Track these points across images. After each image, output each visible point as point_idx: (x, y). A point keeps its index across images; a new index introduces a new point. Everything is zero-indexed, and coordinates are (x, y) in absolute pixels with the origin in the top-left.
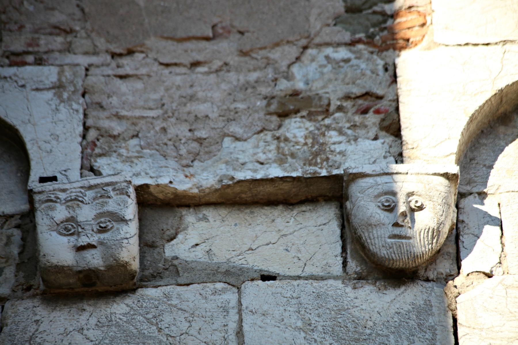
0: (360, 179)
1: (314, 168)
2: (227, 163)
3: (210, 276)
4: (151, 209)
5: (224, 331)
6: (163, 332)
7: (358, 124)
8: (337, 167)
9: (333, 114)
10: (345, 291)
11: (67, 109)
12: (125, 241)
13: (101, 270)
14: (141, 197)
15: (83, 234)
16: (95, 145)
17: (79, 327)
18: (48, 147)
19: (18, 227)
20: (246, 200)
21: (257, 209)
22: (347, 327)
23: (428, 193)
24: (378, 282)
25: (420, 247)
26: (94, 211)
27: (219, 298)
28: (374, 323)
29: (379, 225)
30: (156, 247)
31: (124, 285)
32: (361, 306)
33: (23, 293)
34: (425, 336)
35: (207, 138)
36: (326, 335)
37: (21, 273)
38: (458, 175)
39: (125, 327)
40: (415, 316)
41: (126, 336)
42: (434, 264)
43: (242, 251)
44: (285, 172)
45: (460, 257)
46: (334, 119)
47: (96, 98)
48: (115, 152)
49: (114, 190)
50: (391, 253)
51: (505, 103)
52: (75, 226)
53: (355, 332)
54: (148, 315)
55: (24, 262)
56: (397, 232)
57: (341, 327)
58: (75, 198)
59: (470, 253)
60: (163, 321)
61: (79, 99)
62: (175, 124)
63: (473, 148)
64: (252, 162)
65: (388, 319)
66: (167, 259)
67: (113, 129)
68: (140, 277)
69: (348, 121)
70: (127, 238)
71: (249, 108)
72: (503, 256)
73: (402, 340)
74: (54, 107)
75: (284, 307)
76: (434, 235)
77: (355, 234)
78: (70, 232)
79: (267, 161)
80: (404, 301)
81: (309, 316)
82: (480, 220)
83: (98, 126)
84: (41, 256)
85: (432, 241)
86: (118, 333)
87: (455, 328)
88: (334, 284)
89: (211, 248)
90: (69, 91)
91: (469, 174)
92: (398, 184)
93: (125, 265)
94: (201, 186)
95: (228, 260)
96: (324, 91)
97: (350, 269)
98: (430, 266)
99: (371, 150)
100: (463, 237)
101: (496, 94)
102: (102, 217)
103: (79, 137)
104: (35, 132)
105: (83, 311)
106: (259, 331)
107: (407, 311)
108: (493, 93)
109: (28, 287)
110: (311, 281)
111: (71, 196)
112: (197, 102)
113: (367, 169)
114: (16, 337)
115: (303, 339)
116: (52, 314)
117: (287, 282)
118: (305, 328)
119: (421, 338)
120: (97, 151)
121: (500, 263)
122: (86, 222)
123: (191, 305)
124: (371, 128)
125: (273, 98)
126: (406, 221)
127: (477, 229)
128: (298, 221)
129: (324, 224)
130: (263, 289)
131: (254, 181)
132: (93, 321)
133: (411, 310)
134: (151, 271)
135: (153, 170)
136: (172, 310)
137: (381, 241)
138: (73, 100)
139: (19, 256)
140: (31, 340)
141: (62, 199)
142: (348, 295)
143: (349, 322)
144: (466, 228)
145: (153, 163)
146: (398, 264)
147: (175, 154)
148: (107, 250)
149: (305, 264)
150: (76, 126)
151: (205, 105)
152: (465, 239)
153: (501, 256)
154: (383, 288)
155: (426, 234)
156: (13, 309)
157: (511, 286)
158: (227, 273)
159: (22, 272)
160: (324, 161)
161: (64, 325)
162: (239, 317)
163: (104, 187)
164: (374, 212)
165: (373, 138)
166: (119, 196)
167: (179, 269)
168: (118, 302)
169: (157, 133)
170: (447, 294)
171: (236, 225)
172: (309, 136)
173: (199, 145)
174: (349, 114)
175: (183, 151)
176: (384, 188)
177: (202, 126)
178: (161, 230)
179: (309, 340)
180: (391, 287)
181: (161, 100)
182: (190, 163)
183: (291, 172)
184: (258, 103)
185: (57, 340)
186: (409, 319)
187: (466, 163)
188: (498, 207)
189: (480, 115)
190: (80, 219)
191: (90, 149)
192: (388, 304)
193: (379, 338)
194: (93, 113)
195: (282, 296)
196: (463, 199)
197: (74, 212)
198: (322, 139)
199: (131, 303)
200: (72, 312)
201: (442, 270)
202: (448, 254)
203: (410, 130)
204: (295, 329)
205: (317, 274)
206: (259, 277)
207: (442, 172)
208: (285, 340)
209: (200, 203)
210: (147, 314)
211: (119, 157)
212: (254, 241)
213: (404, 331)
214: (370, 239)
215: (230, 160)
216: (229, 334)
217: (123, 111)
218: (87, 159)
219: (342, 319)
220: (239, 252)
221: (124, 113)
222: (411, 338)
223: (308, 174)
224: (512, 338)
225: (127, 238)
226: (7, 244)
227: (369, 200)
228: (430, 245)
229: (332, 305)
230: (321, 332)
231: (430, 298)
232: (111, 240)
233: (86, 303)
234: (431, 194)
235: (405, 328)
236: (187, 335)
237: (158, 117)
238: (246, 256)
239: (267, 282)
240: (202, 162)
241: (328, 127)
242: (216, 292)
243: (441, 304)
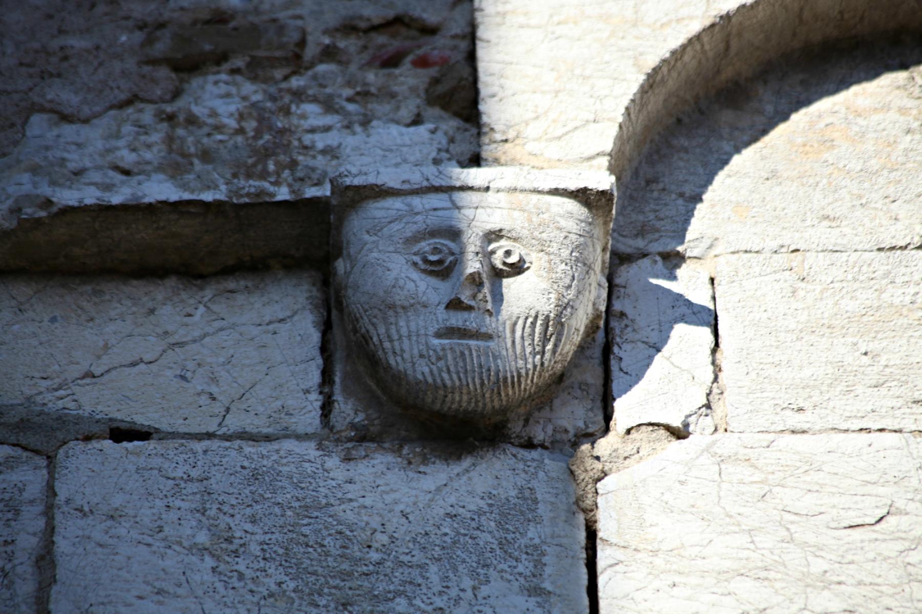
0: (371, 202)
1: (257, 183)
2: (35, 170)
7: (373, 90)
8: (315, 181)
9: (312, 65)
10: (322, 466)
20: (84, 263)
22: (323, 546)
23: (536, 234)
24: (406, 448)
25: (512, 358)
28: (391, 537)
29: (415, 306)
32: (361, 500)
34: (515, 567)
36: (268, 564)
38: (612, 195)
40: (493, 524)
42: (547, 408)
43: (66, 379)
44: (185, 190)
45: (611, 391)
46: (315, 77)
50: (440, 370)
51: (737, 54)
53: (341, 557)
56: (457, 320)
57: (307, 546)
59: (636, 382)
63: (655, 157)
64: (98, 168)
65: (427, 529)
69: (349, 84)
71: (98, 48)
72: (715, 391)
73: (459, 577)
75: (166, 500)
76: (549, 333)
77: (355, 331)
79: (140, 167)
80: (470, 489)
81: (228, 519)
82: (664, 313)
85: (544, 347)
87: (590, 552)
88: (297, 450)
91: (643, 212)
92: (463, 211)
95: (28, 399)
96: (290, 12)
97: (339, 419)
98: (536, 414)
99: (404, 145)
100: (620, 348)
101: (713, 26)
106: (95, 554)
107: (475, 512)
108: (707, 23)
110: (238, 442)
113: (389, 178)
115: (210, 571)
117: (176, 445)
118: (215, 547)
119: (506, 572)
121: (708, 406)
124: (406, 98)
125: (161, 26)
126: (480, 296)
127: (656, 332)
128: (215, 313)
129: (281, 321)
130: (116, 459)
133: (486, 508)
137: (418, 342)
142: (332, 475)
143: (330, 535)
144: (629, 329)
146: (457, 398)
149: (228, 410)
152: (624, 352)
153: (711, 391)
154: (419, 459)
155: (527, 330)
157: (733, 458)
158: (23, 425)
160: (285, 168)
162: (47, 523)
164: (403, 275)
165: (409, 121)
170: (576, 473)
171: (53, 320)
172: (250, 114)
174: (353, 68)
176: (429, 222)
179: (225, 575)
180: (439, 457)
183: (201, 190)
184: (124, 38)
186: (478, 528)
187: (635, 190)
188: (709, 286)
189: (674, 74)
192: (429, 496)
193: (401, 570)
195: (162, 476)
196: (625, 266)
198: (281, 121)
201: (565, 423)
202: (583, 387)
203: (501, 100)
204: (190, 549)
205: (256, 431)
207: (573, 186)
208: (162, 574)
212: (99, 357)
213: (464, 556)
214: (391, 341)
215: (42, 164)
216: (16, 562)
219: (311, 527)
220: (57, 381)
222: (480, 570)
223: (242, 196)
224: (728, 572)
227: (391, 248)
228: (538, 357)
229: (289, 496)
230: (257, 557)
231: (534, 484)
234: (544, 236)
235: (467, 550)
238: (76, 389)
239: (125, 444)
241: (299, 95)
243: (559, 497)
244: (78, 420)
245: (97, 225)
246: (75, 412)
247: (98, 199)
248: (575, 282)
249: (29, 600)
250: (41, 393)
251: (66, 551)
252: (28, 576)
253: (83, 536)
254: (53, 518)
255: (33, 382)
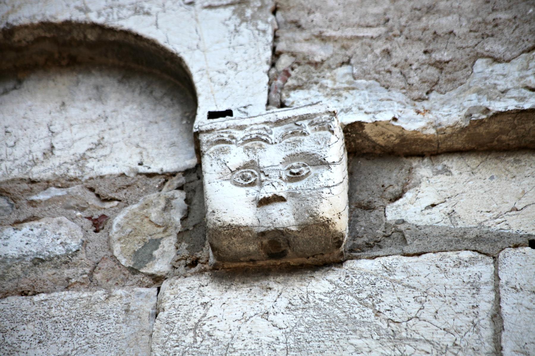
2: (479, 92)
3: (451, 243)
4: (367, 159)
5: (473, 314)
6: (382, 316)
11: (250, 30)
12: (326, 190)
13: (293, 231)
14: (353, 143)
15: (267, 183)
16: (289, 75)
17: (263, 311)
18: (223, 78)
19: (180, 188)
20: (509, 144)
21: (525, 156)
26: (283, 153)
27: (465, 270)
30: (374, 209)
31: (326, 256)
33: (186, 270)
35: (451, 60)
37: (183, 243)
39: (328, 310)
41: (330, 322)
43: (501, 212)
47: (292, 15)
48: (316, 83)
49: (311, 124)
52: (256, 173)
54: (360, 294)
55: (188, 230)
58: (257, 136)
60: (383, 302)
61: (267, 17)
62: (404, 44)
66: (388, 224)
67: (314, 55)
68: (349, 247)
70: (328, 187)
71: (515, 18)
74: (232, 28)
78: (250, 182)
83: (293, 50)
84: (208, 213)
86: (318, 317)
89: (454, 209)
90: (254, 7)
93: (326, 224)
94: (440, 125)
95: (480, 224)
102: (295, 160)
103: (265, 64)
104: (206, 60)
105: (269, 290)
106: (526, 313)
109: (193, 262)
111: (251, 135)
112: (437, 15)
114: (176, 325)
116: (226, 294)
120: (291, 82)
122: (271, 168)
123: (424, 281)
131: (520, 113)
132: (283, 303)
134: (366, 239)
135: (369, 104)
136: (396, 287)
138: (259, 18)
139: (181, 223)
140: (196, 328)
141: (239, 139)
145: (369, 95)
147: (402, 84)
148: (301, 202)
150: (261, 51)
151: (450, 18)
156: (173, 289)
158: (478, 239)
159: (186, 243)
161: (242, 309)
163: (297, 121)
166: (317, 133)
167: (407, 236)
168: (317, 277)
169: (378, 57)
171: (492, 178)
173: (437, 71)
175: (414, 79)
177: (443, 46)
178: (381, 186)
181: (385, 14)
182: (425, 94)
185: (232, 328)
190: (262, 163)
191: (281, 80)
194: (285, 35)
197: (255, 155)
199: (337, 279)
200: (252, 291)
206: (526, 242)
209: (439, 151)
210: (358, 293)
211: (321, 90)
212: (520, 199)
215: (483, 88)
216: (480, 318)
217: (329, 30)
218: (276, 92)
220: (496, 213)
221: (330, 33)
225: (328, 187)
226: (165, 209)
232: (306, 190)
233: (272, 279)
236: (418, 320)
237: (379, 37)
240: (441, 93)
242: (460, 263)
244: (510, 236)
245: (516, 121)
246: (508, 231)
247: (516, 106)
248: (60, 193)
249: (489, 340)
250: (487, 220)
251: (508, 312)
252: (488, 326)
253: (518, 303)
254: (499, 293)
255: (482, 214)
